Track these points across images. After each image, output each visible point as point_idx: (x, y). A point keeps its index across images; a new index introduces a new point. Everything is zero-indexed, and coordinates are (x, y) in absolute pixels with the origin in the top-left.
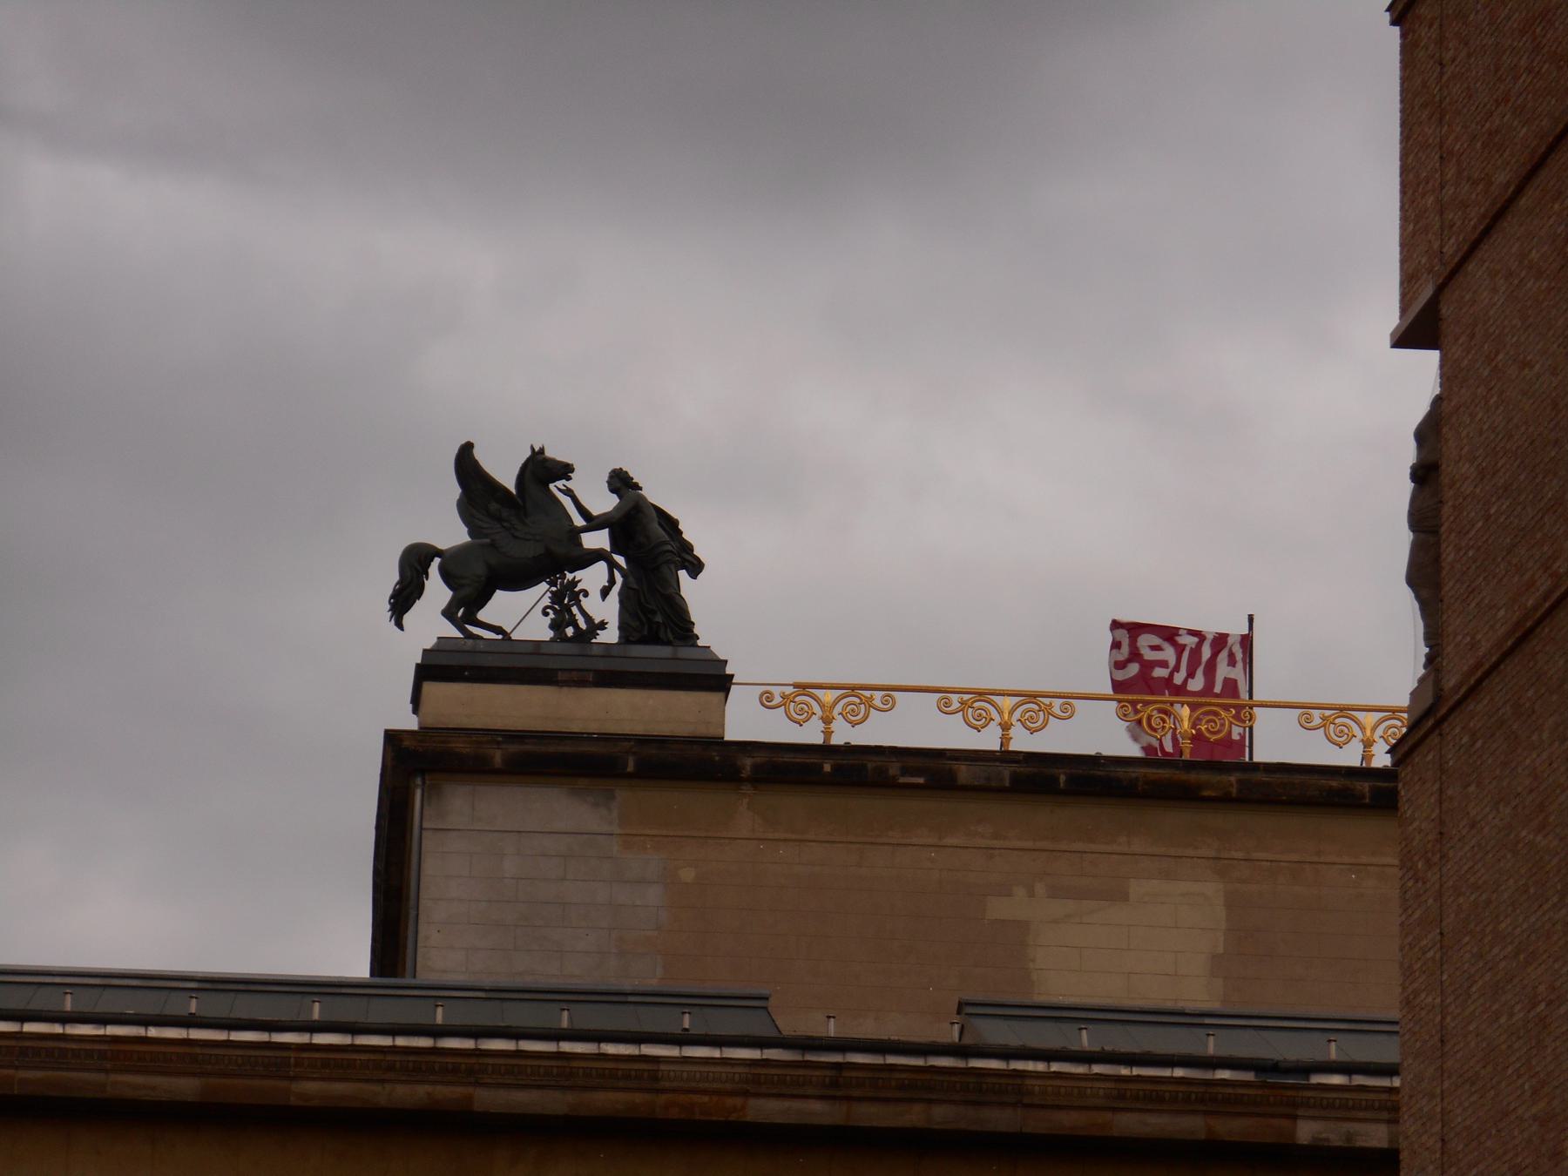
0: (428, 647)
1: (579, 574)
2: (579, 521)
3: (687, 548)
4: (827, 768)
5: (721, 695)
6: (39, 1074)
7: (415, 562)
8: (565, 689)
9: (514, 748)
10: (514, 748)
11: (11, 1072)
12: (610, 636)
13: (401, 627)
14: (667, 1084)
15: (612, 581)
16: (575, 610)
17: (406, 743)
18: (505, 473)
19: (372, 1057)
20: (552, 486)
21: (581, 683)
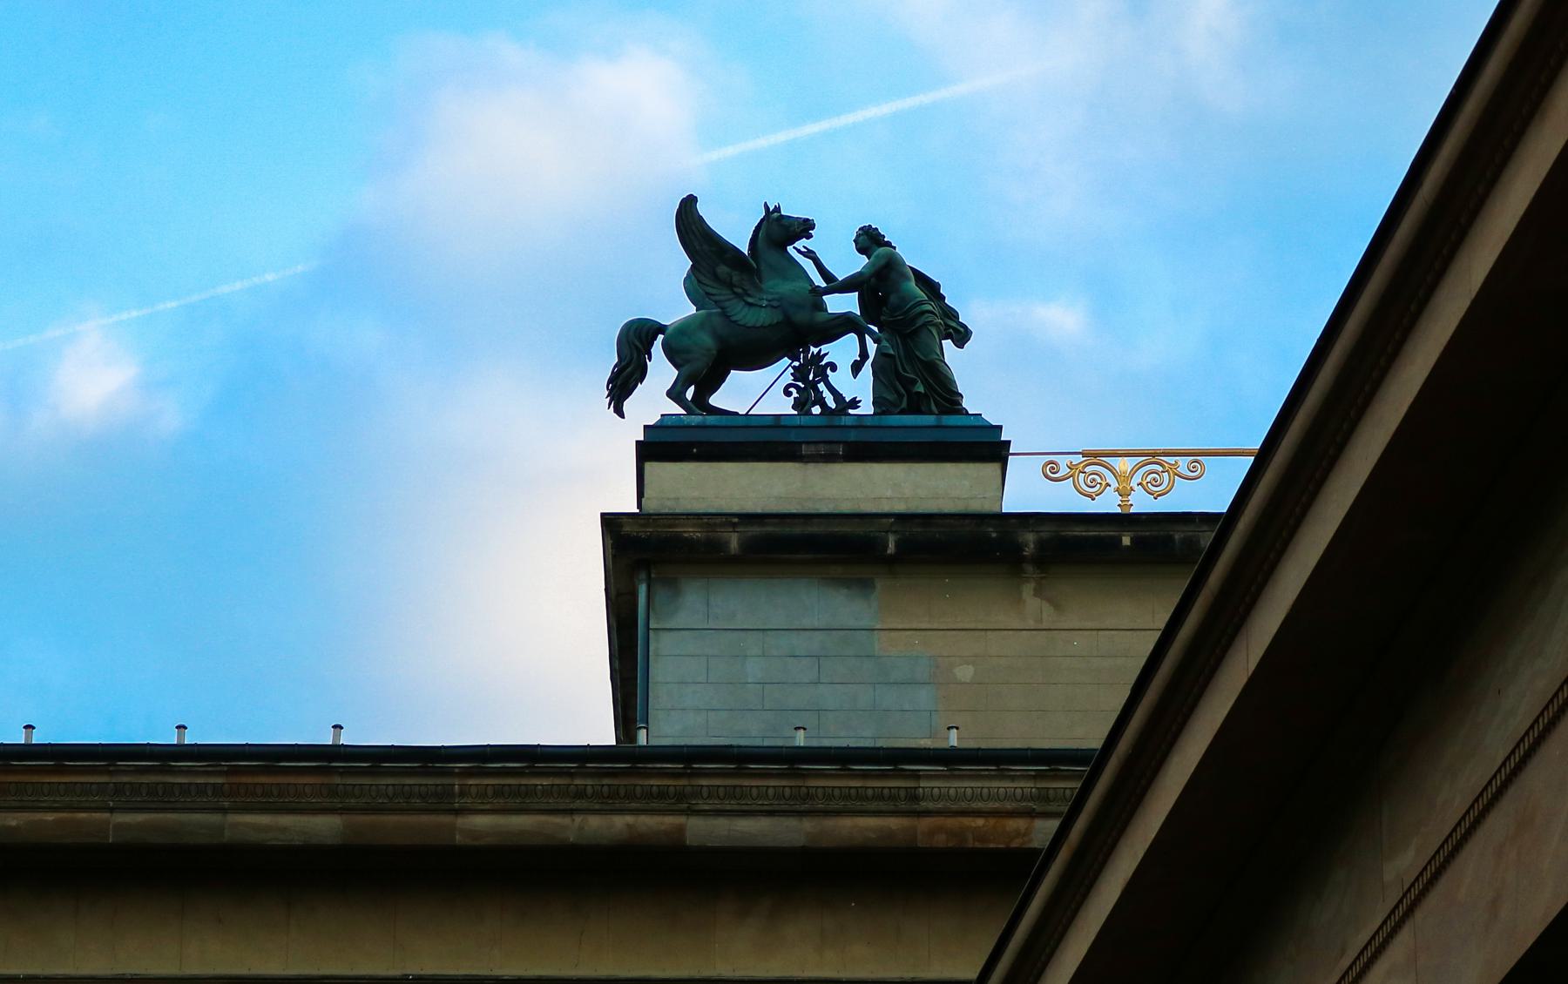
0: (651, 423)
1: (825, 348)
2: (819, 281)
3: (951, 314)
4: (1126, 541)
5: (994, 468)
6: (140, 818)
7: (636, 343)
8: (811, 466)
9: (755, 530)
10: (755, 530)
11: (106, 815)
12: (866, 408)
13: (622, 415)
14: (931, 806)
15: (864, 354)
16: (821, 386)
17: (627, 529)
18: (738, 234)
19: (557, 781)
20: (790, 249)
21: (830, 458)
